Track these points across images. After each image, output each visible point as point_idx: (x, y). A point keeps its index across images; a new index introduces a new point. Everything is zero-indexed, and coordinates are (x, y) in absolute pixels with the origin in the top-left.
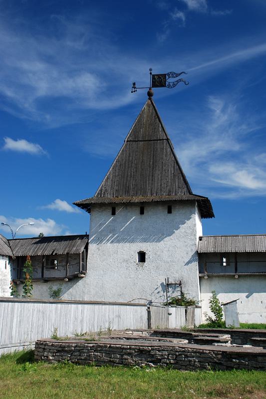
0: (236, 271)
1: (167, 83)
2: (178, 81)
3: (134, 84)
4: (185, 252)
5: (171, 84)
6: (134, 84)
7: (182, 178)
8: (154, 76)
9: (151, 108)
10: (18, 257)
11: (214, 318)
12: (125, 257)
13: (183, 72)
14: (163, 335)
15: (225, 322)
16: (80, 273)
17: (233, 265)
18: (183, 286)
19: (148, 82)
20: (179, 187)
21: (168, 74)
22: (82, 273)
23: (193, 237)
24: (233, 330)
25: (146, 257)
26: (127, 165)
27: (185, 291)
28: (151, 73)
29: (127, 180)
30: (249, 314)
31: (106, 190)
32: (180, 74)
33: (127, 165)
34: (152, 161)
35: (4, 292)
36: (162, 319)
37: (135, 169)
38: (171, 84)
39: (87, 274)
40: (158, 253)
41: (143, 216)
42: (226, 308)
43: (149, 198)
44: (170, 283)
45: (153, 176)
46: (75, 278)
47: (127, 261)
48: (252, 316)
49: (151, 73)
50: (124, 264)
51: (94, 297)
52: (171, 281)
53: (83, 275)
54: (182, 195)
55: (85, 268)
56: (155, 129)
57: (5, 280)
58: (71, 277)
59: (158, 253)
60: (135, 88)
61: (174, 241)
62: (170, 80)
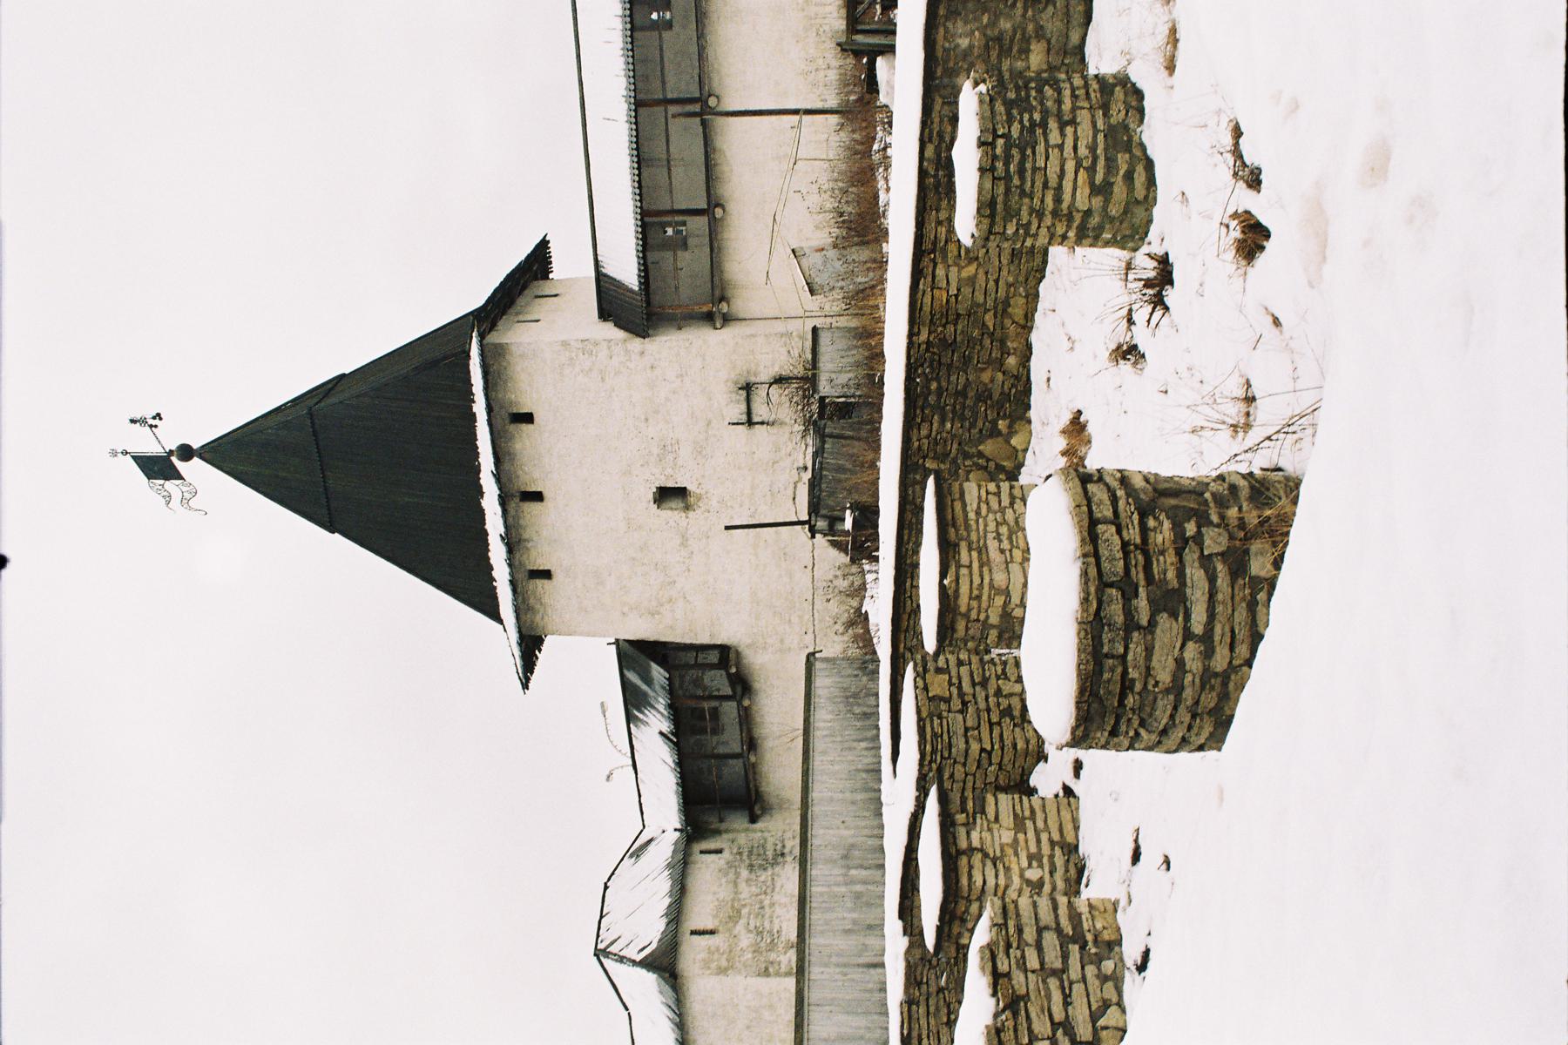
18: (753, 379)
27: (765, 375)
35: (783, 855)
41: (546, 494)
52: (738, 411)
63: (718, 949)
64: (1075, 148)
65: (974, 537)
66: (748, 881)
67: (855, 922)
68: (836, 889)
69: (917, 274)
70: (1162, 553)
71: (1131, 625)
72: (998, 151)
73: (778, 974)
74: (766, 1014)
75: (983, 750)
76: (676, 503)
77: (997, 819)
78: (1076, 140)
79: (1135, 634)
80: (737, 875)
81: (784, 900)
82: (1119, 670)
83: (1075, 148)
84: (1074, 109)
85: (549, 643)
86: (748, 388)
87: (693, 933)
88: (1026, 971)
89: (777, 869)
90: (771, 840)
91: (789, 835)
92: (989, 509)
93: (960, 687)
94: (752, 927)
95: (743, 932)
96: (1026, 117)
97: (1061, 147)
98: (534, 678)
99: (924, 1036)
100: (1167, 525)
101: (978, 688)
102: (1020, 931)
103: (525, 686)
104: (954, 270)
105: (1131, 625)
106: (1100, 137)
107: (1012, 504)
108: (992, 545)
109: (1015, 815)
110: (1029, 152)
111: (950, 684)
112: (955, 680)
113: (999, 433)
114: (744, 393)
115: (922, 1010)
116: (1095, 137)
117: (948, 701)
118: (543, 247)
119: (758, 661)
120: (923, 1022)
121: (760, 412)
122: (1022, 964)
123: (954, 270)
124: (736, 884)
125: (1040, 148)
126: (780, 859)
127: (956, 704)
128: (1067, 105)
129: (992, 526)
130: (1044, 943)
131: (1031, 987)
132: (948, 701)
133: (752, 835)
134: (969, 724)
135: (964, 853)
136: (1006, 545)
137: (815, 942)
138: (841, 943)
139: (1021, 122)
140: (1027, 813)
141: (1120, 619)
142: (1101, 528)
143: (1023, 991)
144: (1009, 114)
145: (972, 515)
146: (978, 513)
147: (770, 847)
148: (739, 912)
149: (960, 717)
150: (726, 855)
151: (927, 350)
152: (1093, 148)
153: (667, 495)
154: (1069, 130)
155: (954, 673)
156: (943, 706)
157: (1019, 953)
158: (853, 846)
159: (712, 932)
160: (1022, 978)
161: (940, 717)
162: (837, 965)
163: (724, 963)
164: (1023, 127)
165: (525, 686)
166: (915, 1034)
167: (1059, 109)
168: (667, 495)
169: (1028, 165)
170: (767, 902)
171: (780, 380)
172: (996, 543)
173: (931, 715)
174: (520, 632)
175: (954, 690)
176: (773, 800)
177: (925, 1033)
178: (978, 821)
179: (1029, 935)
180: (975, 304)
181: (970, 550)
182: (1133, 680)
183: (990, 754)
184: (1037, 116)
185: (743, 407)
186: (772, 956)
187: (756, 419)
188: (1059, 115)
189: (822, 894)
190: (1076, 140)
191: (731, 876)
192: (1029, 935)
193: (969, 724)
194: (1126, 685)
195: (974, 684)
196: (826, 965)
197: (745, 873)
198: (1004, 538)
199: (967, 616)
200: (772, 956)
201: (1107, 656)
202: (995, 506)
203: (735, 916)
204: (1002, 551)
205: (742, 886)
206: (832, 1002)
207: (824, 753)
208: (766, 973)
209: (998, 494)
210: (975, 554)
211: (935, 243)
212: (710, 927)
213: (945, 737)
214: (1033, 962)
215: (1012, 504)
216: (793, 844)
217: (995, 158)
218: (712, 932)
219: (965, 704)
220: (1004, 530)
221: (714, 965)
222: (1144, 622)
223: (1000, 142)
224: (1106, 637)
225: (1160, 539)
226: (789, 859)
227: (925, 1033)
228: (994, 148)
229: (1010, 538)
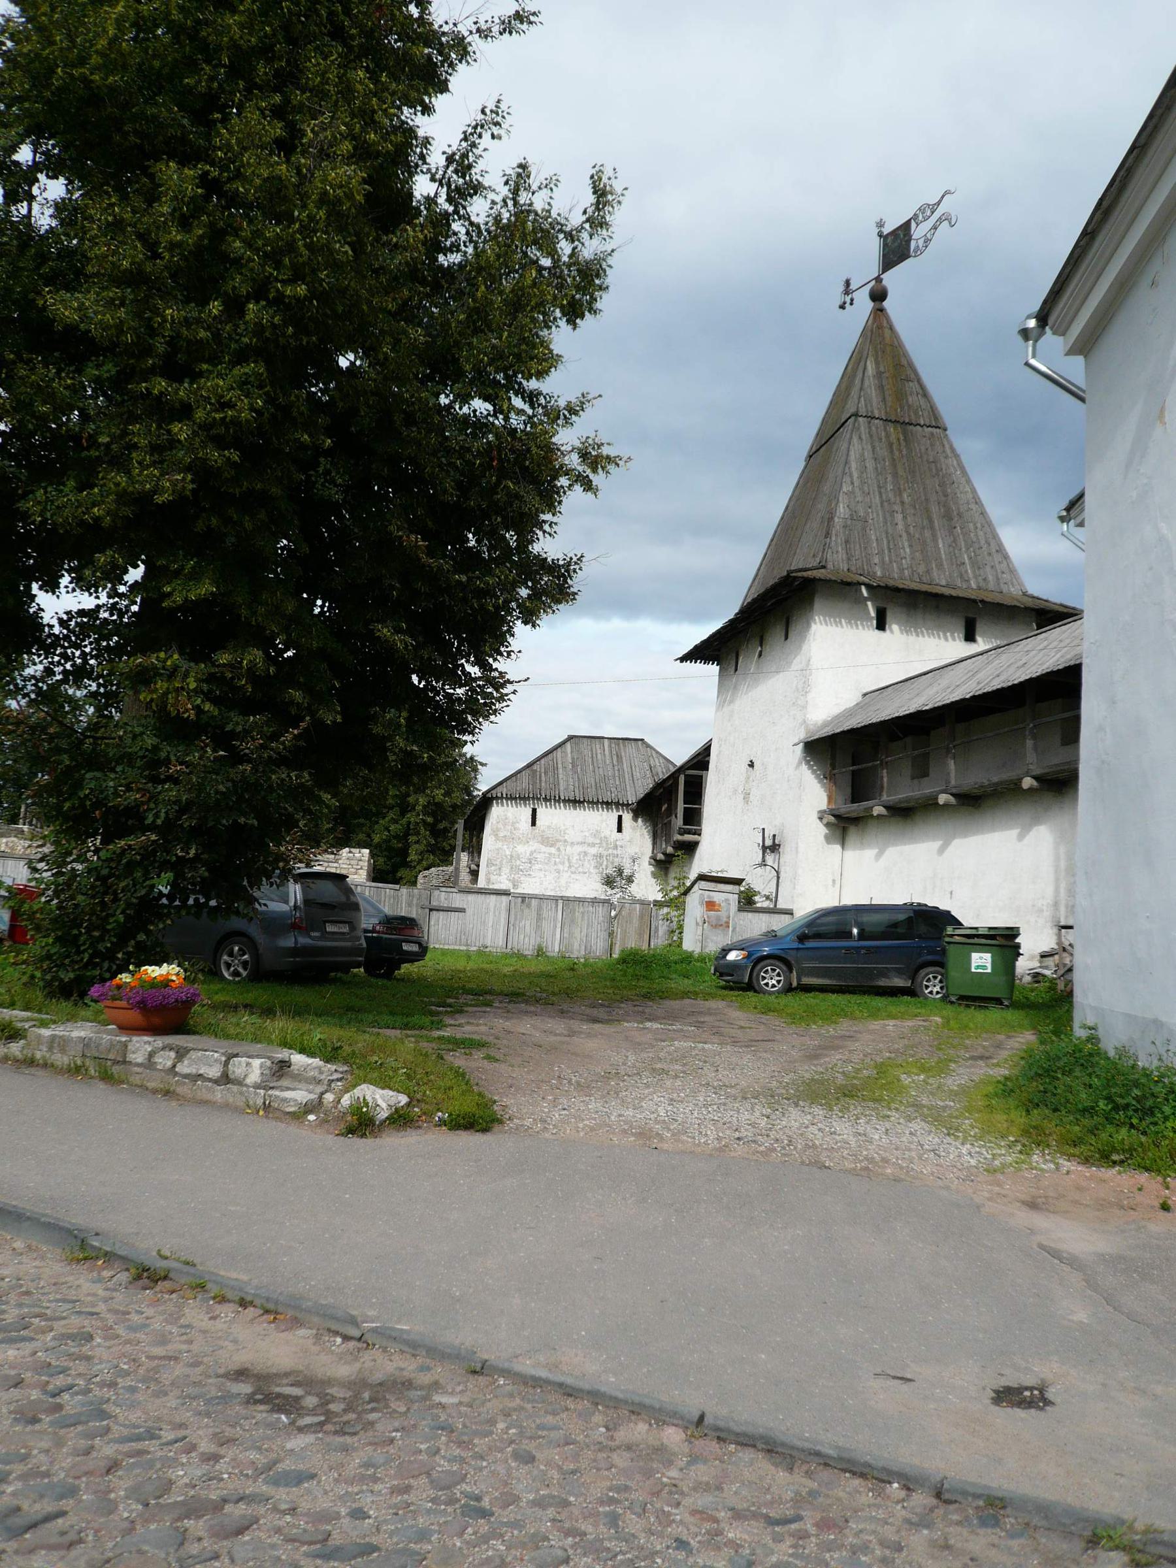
32: (939, 203)
66: (586, 854)
81: (563, 882)
87: (534, 811)
95: (533, 849)
103: (683, 659)
163: (501, 834)
165: (683, 659)
170: (561, 867)
186: (506, 870)
191: (591, 840)
200: (506, 870)
205: (579, 849)
221: (500, 826)
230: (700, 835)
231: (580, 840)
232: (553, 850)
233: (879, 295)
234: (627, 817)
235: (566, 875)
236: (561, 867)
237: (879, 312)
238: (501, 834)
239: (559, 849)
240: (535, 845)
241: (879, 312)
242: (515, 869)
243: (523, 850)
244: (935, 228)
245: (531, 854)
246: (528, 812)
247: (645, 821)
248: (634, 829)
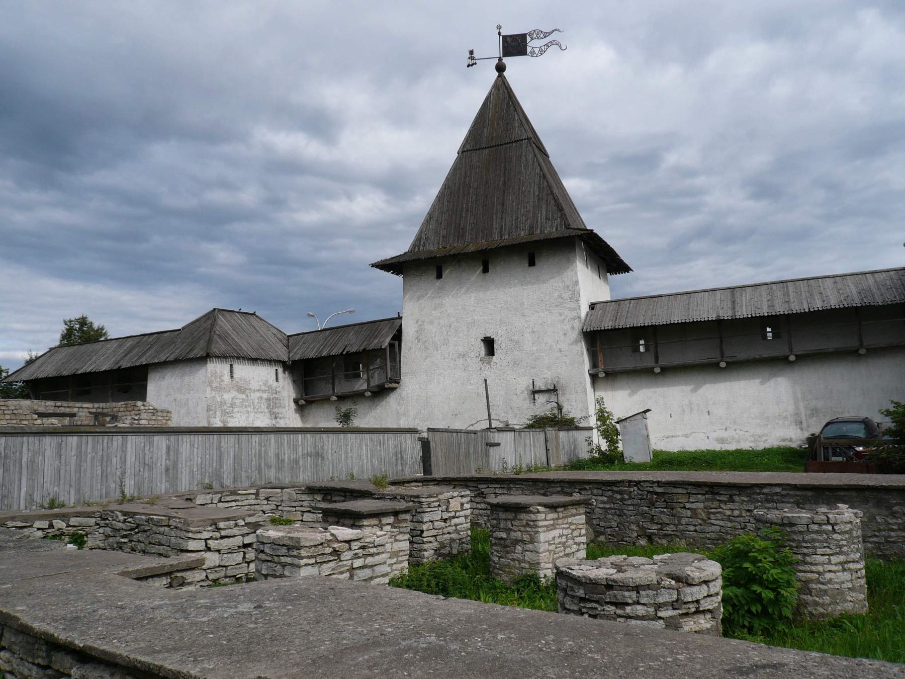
0: (657, 361)
1: (529, 49)
2: (547, 46)
3: (471, 52)
4: (562, 333)
5: (537, 50)
6: (471, 52)
7: (552, 202)
8: (505, 37)
9: (501, 91)
10: (294, 362)
11: (604, 446)
12: (461, 349)
13: (556, 30)
14: (326, 495)
15: (622, 453)
16: (387, 381)
17: (652, 348)
18: (560, 392)
19: (495, 48)
20: (547, 219)
21: (530, 34)
22: (392, 381)
23: (573, 305)
24: (520, 477)
25: (496, 346)
26: (461, 191)
27: (562, 399)
28: (499, 34)
29: (461, 217)
30: (686, 436)
31: (427, 239)
32: (550, 33)
33: (461, 191)
34: (502, 179)
35: (276, 418)
36: (467, 455)
37: (474, 198)
38: (537, 50)
39: (401, 383)
40: (515, 338)
41: (488, 274)
42: (625, 427)
43: (496, 239)
44: (537, 388)
45: (503, 205)
46: (381, 392)
47: (463, 356)
48: (690, 438)
49: (499, 34)
50: (460, 362)
51: (415, 419)
52: (540, 385)
53: (394, 385)
54: (552, 230)
55: (397, 370)
56: (508, 124)
57: (277, 399)
58: (375, 390)
59: (515, 338)
60: (473, 59)
61: (542, 315)
62: (533, 44)
63: (222, 381)
64: (830, 571)
65: (560, 521)
66: (261, 398)
67: (283, 461)
68: (300, 449)
69: (698, 485)
70: (695, 622)
71: (658, 607)
72: (824, 527)
73: (209, 417)
74: (183, 411)
75: (422, 532)
76: (483, 351)
77: (396, 541)
78: (835, 572)
79: (652, 609)
80: (264, 391)
81: (251, 419)
82: (630, 601)
83: (830, 571)
84: (850, 570)
85: (399, 279)
86: (553, 390)
87: (231, 365)
88: (352, 559)
89: (268, 415)
90: (284, 411)
91: (287, 422)
92: (573, 530)
93: (454, 517)
94: (235, 401)
95: (233, 395)
96: (845, 543)
97: (830, 563)
98: (383, 273)
99: (238, 503)
100: (709, 626)
101: (454, 528)
102: (372, 555)
103: (373, 266)
104: (702, 505)
105: (658, 607)
106: (837, 586)
107: (576, 543)
108: (556, 533)
109: (399, 552)
110: (825, 544)
111: (456, 512)
112: (458, 514)
113: (596, 536)
114: (552, 388)
115: (253, 502)
116: (837, 583)
117: (447, 510)
118: (625, 268)
119: (392, 400)
120: (246, 502)
121: (541, 399)
122: (356, 557)
123: (702, 505)
124: (259, 390)
125: (828, 551)
126: (273, 416)
127: (446, 515)
128: (852, 566)
129: (566, 532)
130: (366, 570)
131: (345, 563)
132: (447, 510)
133: (286, 399)
134: (436, 523)
135: (380, 521)
136: (557, 541)
137: (229, 441)
138: (272, 453)
139: (842, 540)
140: (400, 559)
141: (661, 600)
142: (705, 586)
143: (342, 558)
144: (846, 532)
145: (570, 520)
146: (571, 524)
147: (281, 410)
148: (244, 393)
149: (439, 518)
150: (275, 384)
151: (649, 492)
152: (830, 581)
153: (489, 344)
154: (840, 568)
155: (462, 513)
156: (444, 507)
157: (361, 555)
158: (323, 458)
159: (232, 377)
160: (349, 557)
161: (439, 506)
162: (260, 451)
163: (214, 385)
164: (839, 541)
165: (373, 266)
166: (238, 498)
167: (850, 562)
168: (489, 344)
169: (817, 544)
170: (249, 409)
171: (560, 408)
172: (557, 535)
173: (439, 501)
174: (403, 262)
175: (453, 514)
176: (306, 411)
177: (240, 503)
178: (395, 530)
179: (369, 560)
180: (680, 518)
181: (553, 519)
182: (625, 609)
183: (420, 536)
184: (845, 549)
185: (543, 388)
186: (219, 413)
187: (536, 396)
188: (847, 562)
189: (297, 441)
190: (835, 572)
191: (263, 388)
192: (369, 560)
193: (436, 523)
194: (622, 605)
195: (456, 525)
196: (260, 444)
197: (265, 396)
198: (560, 540)
199: (515, 519)
200: (219, 413)
201: (638, 593)
202: (576, 533)
203: (241, 390)
204: (554, 538)
205: (258, 394)
206: (240, 448)
207: (372, 440)
208: (208, 410)
209: (580, 535)
210: (552, 522)
211: (718, 494)
212: (235, 376)
213: (429, 509)
214: (358, 563)
215: (576, 543)
216: (282, 424)
217: (820, 525)
218: (232, 377)
219: (445, 520)
220: (564, 539)
221: (213, 379)
222: (660, 614)
223: (830, 528)
224: (651, 592)
225: (702, 621)
226: (274, 422)
227: (240, 503)
228: (825, 524)
229: (560, 543)
230: (398, 383)
231: (258, 388)
232: (244, 396)
233: (501, 68)
234: (280, 370)
235: (252, 414)
236: (249, 409)
237: (501, 76)
238: (214, 385)
239: (247, 396)
240: (234, 393)
241: (501, 76)
242: (224, 413)
243: (227, 397)
244: (547, 46)
245: (232, 399)
246: (228, 367)
247: (289, 373)
248: (284, 379)
